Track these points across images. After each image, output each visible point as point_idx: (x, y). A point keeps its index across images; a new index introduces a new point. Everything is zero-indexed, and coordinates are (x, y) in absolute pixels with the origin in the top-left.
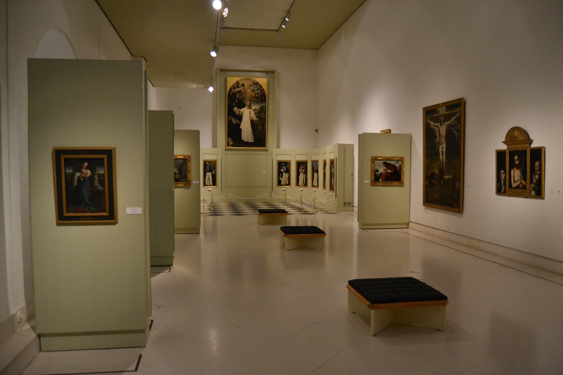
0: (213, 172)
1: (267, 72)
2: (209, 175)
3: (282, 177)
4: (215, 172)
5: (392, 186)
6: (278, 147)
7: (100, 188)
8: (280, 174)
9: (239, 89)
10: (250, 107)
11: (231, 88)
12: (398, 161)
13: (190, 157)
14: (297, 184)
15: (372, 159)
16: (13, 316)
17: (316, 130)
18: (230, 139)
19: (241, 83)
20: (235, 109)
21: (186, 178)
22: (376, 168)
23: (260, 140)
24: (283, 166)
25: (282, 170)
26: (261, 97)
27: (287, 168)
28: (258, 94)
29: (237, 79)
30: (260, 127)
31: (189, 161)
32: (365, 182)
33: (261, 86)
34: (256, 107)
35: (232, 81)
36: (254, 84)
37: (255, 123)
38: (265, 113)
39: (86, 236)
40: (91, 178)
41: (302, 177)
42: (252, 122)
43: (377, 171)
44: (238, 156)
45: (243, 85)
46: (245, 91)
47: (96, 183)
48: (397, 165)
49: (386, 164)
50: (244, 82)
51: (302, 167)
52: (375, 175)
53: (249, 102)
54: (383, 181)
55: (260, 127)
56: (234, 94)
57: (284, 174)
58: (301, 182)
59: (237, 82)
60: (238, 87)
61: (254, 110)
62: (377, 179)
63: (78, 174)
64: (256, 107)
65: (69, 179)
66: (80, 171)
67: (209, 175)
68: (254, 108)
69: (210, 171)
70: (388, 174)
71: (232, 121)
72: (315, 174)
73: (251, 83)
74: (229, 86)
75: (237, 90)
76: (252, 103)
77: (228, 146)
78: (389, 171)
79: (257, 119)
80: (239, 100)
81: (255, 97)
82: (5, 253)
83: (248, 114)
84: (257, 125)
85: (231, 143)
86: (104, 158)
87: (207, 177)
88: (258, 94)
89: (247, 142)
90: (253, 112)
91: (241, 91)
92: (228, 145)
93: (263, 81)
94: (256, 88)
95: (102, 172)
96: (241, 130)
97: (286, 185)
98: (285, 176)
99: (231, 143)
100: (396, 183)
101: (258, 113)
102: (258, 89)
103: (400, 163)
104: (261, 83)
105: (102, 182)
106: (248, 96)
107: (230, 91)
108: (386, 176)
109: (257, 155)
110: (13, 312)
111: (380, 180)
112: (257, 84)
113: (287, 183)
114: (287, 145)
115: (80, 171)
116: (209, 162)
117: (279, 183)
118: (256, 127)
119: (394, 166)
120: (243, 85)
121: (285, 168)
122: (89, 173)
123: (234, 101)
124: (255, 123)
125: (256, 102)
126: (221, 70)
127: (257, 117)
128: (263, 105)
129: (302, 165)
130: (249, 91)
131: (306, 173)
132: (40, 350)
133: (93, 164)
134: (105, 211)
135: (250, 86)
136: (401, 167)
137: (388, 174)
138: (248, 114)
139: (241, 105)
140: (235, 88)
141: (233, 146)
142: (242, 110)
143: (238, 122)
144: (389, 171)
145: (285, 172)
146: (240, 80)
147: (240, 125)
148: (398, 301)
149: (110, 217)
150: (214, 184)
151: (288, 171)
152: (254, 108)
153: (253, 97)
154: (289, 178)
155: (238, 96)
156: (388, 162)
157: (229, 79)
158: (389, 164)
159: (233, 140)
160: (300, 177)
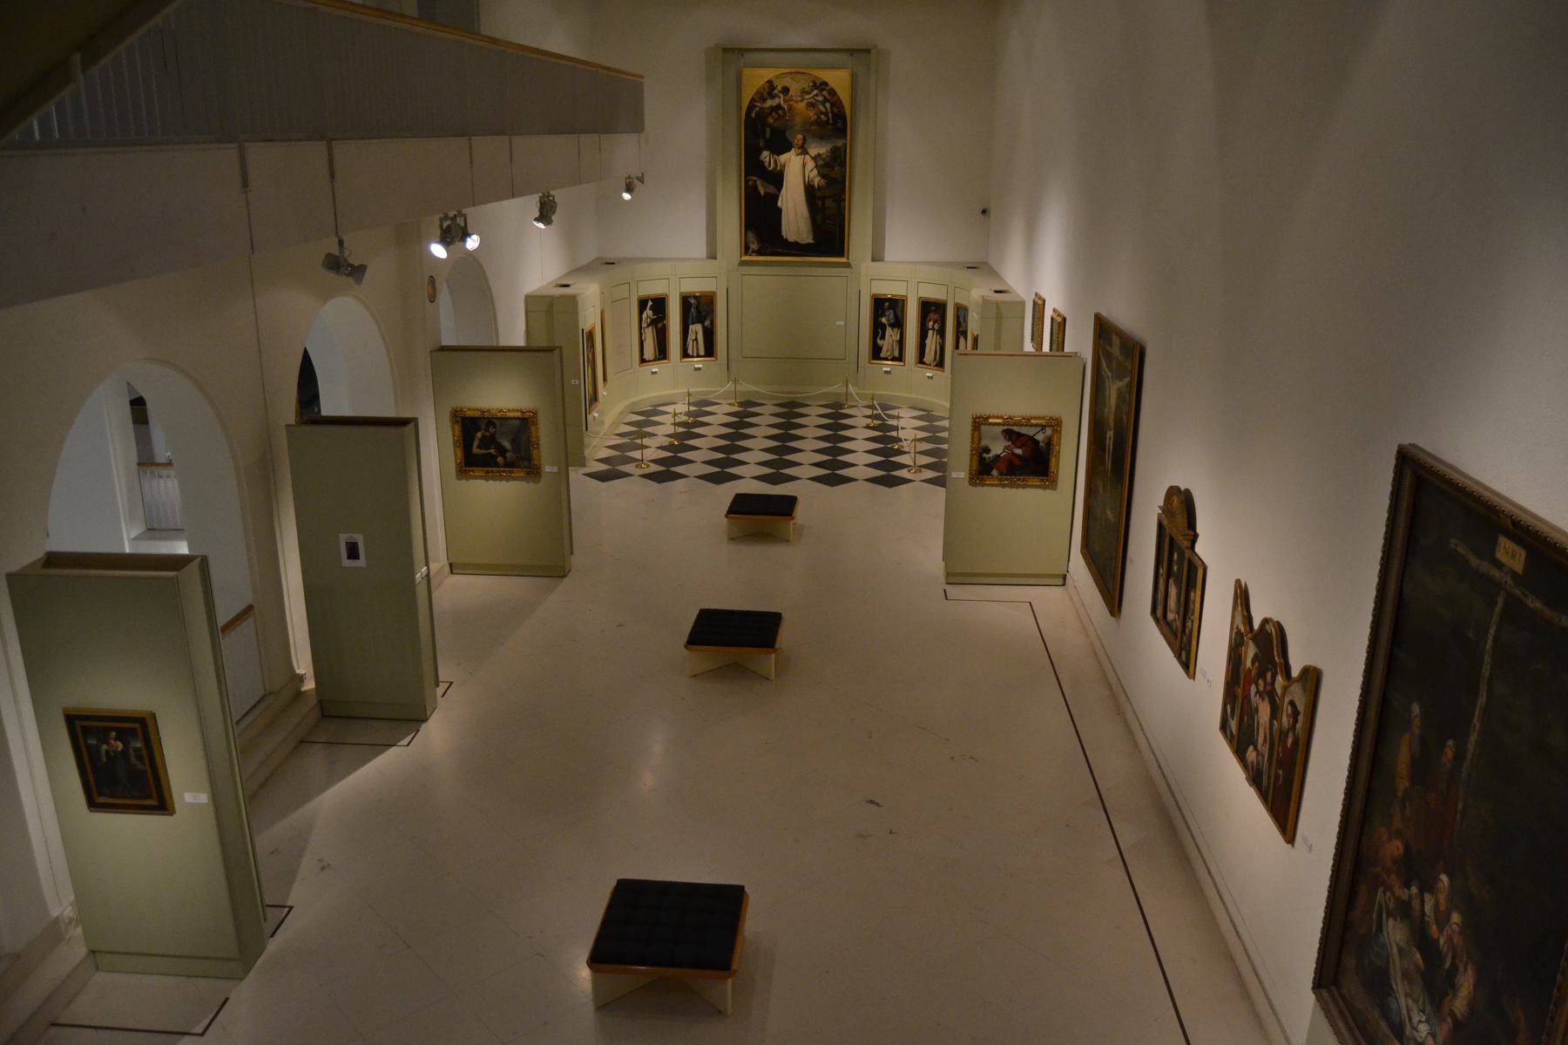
0: (707, 323)
1: (851, 52)
2: (696, 329)
3: (883, 338)
4: (712, 322)
5: (1025, 486)
6: (877, 257)
7: (140, 766)
8: (878, 330)
9: (774, 102)
10: (804, 151)
11: (753, 100)
12: (1043, 427)
13: (535, 414)
14: (921, 359)
15: (974, 422)
16: (56, 921)
17: (984, 212)
18: (751, 236)
19: (779, 85)
20: (765, 155)
21: (529, 460)
22: (984, 443)
23: (829, 237)
24: (886, 310)
25: (884, 320)
26: (834, 123)
27: (896, 316)
28: (826, 114)
29: (768, 74)
30: (829, 203)
31: (535, 424)
32: (954, 475)
33: (832, 92)
34: (819, 149)
35: (756, 78)
36: (815, 86)
37: (818, 194)
38: (843, 165)
39: (127, 830)
40: (125, 753)
41: (932, 341)
42: (809, 189)
43: (987, 450)
44: (770, 281)
45: (786, 90)
46: (790, 107)
47: (133, 760)
48: (1040, 437)
49: (1010, 434)
50: (787, 82)
51: (932, 315)
52: (981, 460)
53: (800, 137)
54: (1001, 473)
55: (829, 203)
56: (762, 115)
57: (889, 330)
58: (929, 356)
59: (770, 82)
60: (773, 97)
61: (814, 158)
62: (983, 469)
63: (105, 747)
64: (819, 149)
65: (93, 753)
66: (108, 744)
67: (696, 329)
68: (813, 151)
69: (700, 320)
70: (1016, 461)
71: (755, 187)
72: (962, 340)
73: (806, 84)
74: (748, 94)
75: (770, 103)
76: (809, 140)
77: (746, 253)
78: (1019, 451)
79: (823, 182)
80: (773, 130)
81: (818, 122)
82: (29, 840)
83: (797, 170)
84: (823, 198)
85: (755, 246)
86: (140, 729)
87: (691, 337)
88: (826, 114)
89: (796, 243)
90: (811, 164)
91: (779, 107)
92: (747, 250)
93: (838, 79)
94: (820, 98)
95: (139, 745)
96: (780, 210)
97: (894, 359)
98: (891, 335)
99: (755, 246)
100: (1035, 481)
101: (826, 165)
102: (826, 100)
103: (1049, 431)
104: (832, 84)
105: (140, 758)
106: (798, 120)
107: (751, 108)
108: (1010, 462)
109: (820, 278)
110: (55, 913)
111: (995, 472)
112: (821, 86)
113: (896, 354)
114: (902, 253)
115: (108, 744)
116: (695, 297)
117: (876, 353)
118: (819, 203)
119: (1032, 439)
120: (786, 90)
121: (890, 314)
122: (120, 746)
123: (762, 133)
124: (818, 194)
125: (821, 138)
126: (725, 50)
127: (822, 175)
128: (840, 143)
129: (931, 310)
130: (802, 105)
131: (941, 333)
132: (97, 969)
133: (123, 735)
134: (150, 797)
135: (804, 92)
136: (1049, 443)
137: (1016, 461)
138: (797, 170)
139: (782, 146)
140: (764, 100)
141: (759, 253)
142: (783, 158)
143: (772, 189)
144: (1019, 451)
145: (892, 326)
146: (777, 77)
147: (776, 197)
148: (671, 936)
149: (161, 804)
150: (710, 351)
151: (899, 324)
152: (813, 151)
153: (811, 124)
154: (901, 343)
155: (771, 120)
156: (1016, 429)
157: (747, 72)
158: (1019, 435)
159: (761, 238)
160: (928, 342)
